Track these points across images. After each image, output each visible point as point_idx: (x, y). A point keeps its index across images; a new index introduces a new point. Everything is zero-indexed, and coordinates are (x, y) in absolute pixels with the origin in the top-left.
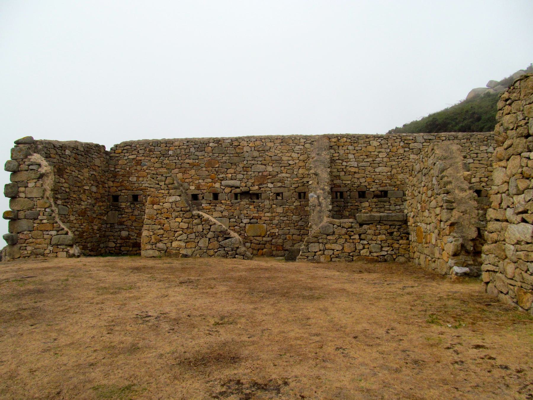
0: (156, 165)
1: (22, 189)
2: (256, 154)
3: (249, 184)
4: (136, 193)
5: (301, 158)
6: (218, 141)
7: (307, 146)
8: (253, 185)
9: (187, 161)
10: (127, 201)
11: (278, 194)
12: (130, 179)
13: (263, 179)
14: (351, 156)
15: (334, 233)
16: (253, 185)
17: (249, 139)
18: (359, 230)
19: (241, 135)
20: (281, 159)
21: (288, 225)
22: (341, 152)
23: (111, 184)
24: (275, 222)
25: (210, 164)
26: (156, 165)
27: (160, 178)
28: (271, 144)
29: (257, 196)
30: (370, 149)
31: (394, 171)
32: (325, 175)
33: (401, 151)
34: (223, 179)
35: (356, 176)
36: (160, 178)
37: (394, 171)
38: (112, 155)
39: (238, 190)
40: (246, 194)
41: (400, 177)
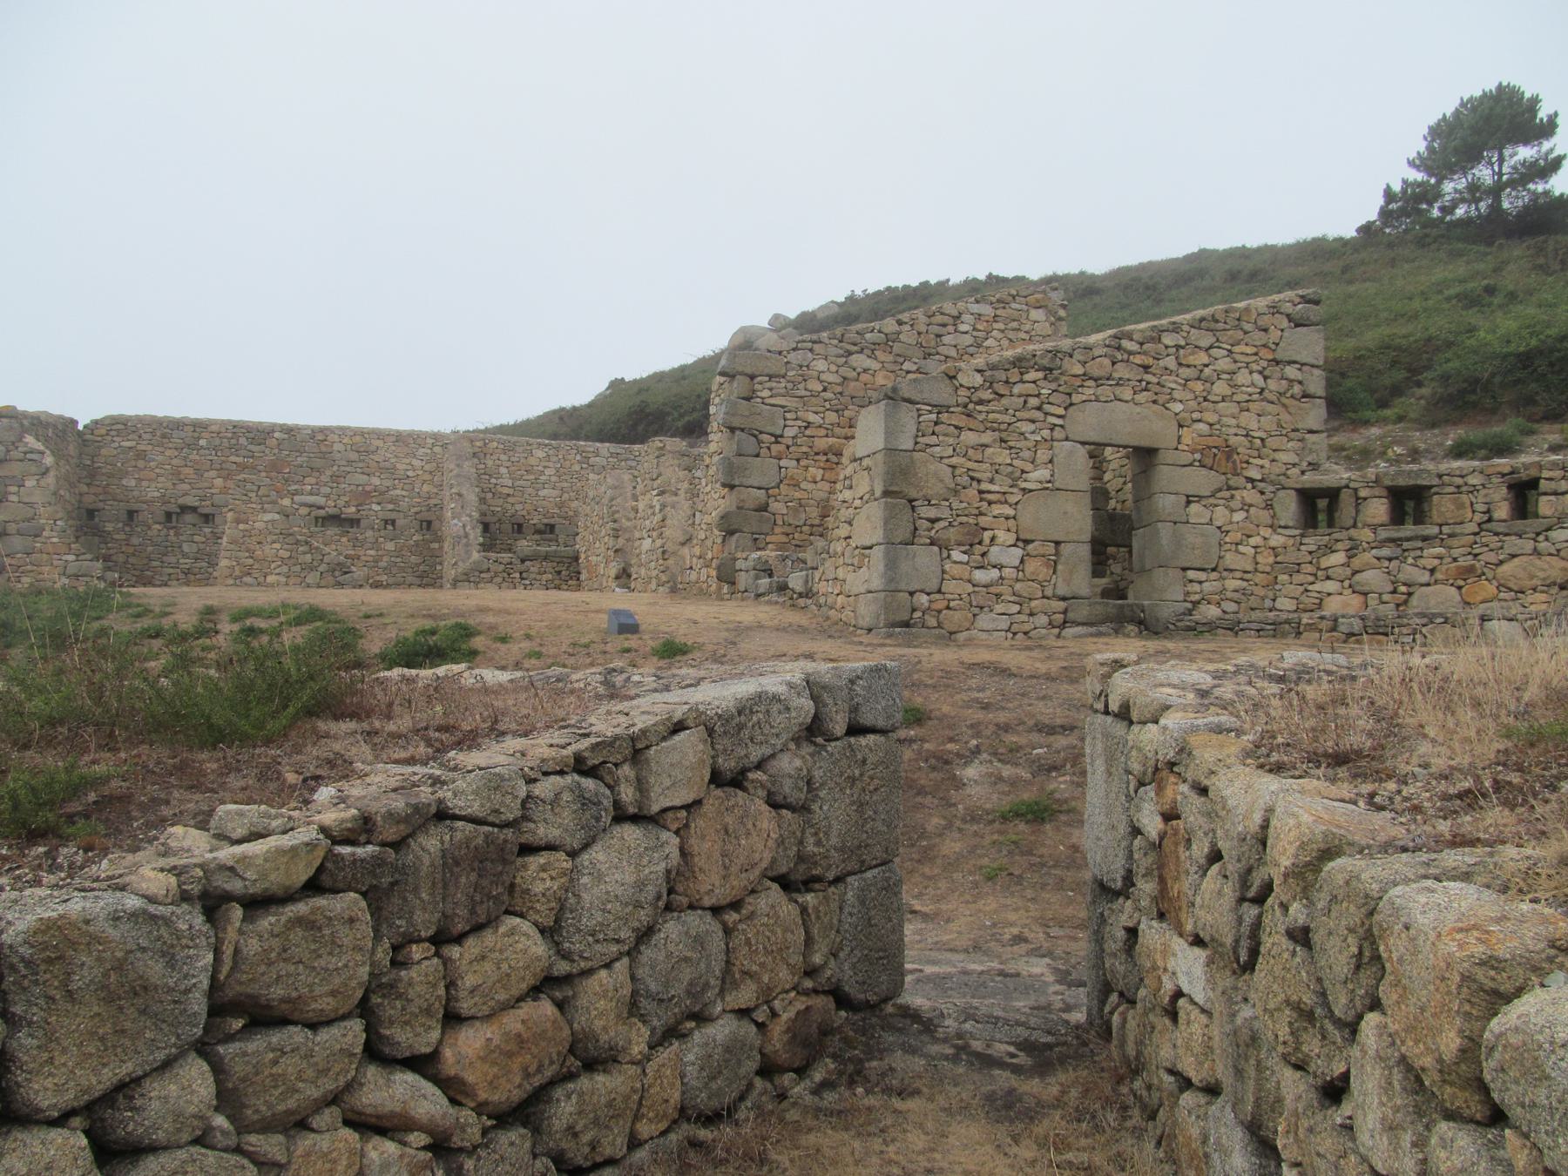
0: (175, 462)
1: (14, 489)
2: (354, 456)
3: (341, 503)
4: (135, 507)
5: (427, 467)
6: (290, 431)
7: (437, 449)
8: (347, 504)
9: (233, 458)
10: (118, 520)
11: (386, 522)
12: (124, 482)
13: (365, 496)
14: (503, 470)
15: (489, 570)
16: (347, 504)
17: (343, 431)
18: (520, 567)
19: (327, 424)
20: (394, 468)
21: (403, 570)
22: (490, 463)
23: (85, 489)
24: (383, 564)
25: (274, 467)
26: (175, 462)
27: (249, 486)
28: (380, 443)
29: (354, 522)
30: (532, 461)
31: (566, 496)
32: (472, 497)
33: (577, 467)
34: (296, 493)
35: (510, 500)
36: (249, 486)
37: (566, 496)
38: (89, 437)
39: (322, 513)
40: (335, 519)
41: (575, 504)
